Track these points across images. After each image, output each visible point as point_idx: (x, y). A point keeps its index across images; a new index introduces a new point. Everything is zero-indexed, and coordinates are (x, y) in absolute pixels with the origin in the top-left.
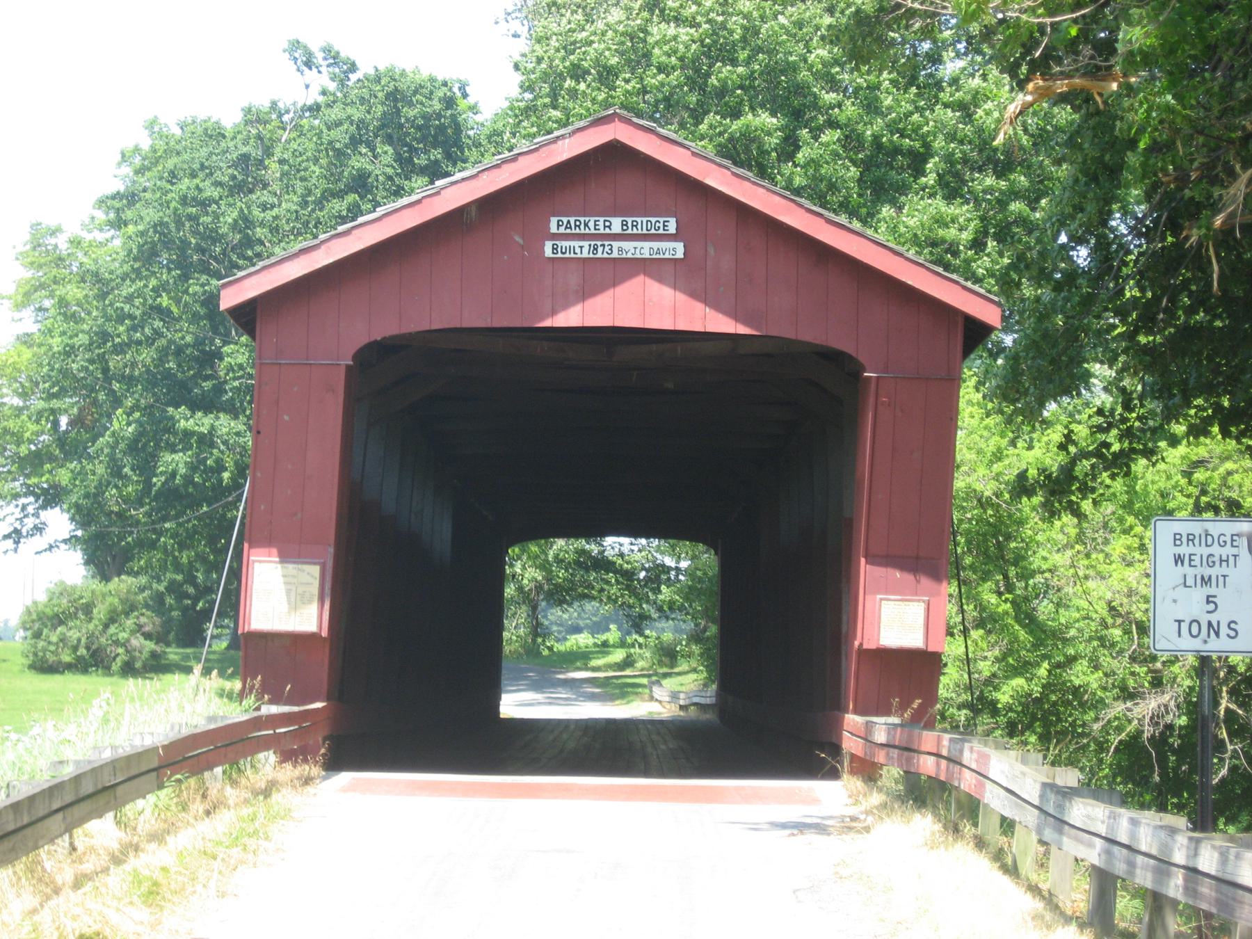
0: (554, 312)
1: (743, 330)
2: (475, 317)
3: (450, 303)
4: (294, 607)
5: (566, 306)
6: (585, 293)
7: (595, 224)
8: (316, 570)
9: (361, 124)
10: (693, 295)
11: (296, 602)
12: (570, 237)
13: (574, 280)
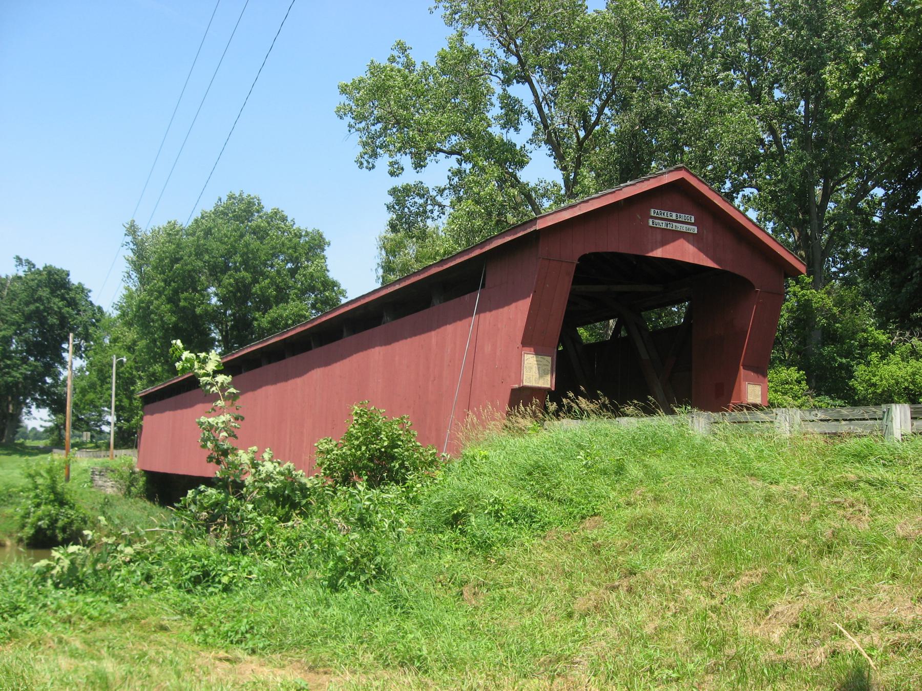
0: (652, 250)
1: (716, 266)
2: (623, 249)
3: (613, 241)
4: (541, 376)
5: (656, 248)
6: (663, 243)
7: (666, 214)
8: (549, 359)
9: (40, 281)
10: (699, 249)
11: (542, 374)
12: (660, 218)
13: (659, 237)
